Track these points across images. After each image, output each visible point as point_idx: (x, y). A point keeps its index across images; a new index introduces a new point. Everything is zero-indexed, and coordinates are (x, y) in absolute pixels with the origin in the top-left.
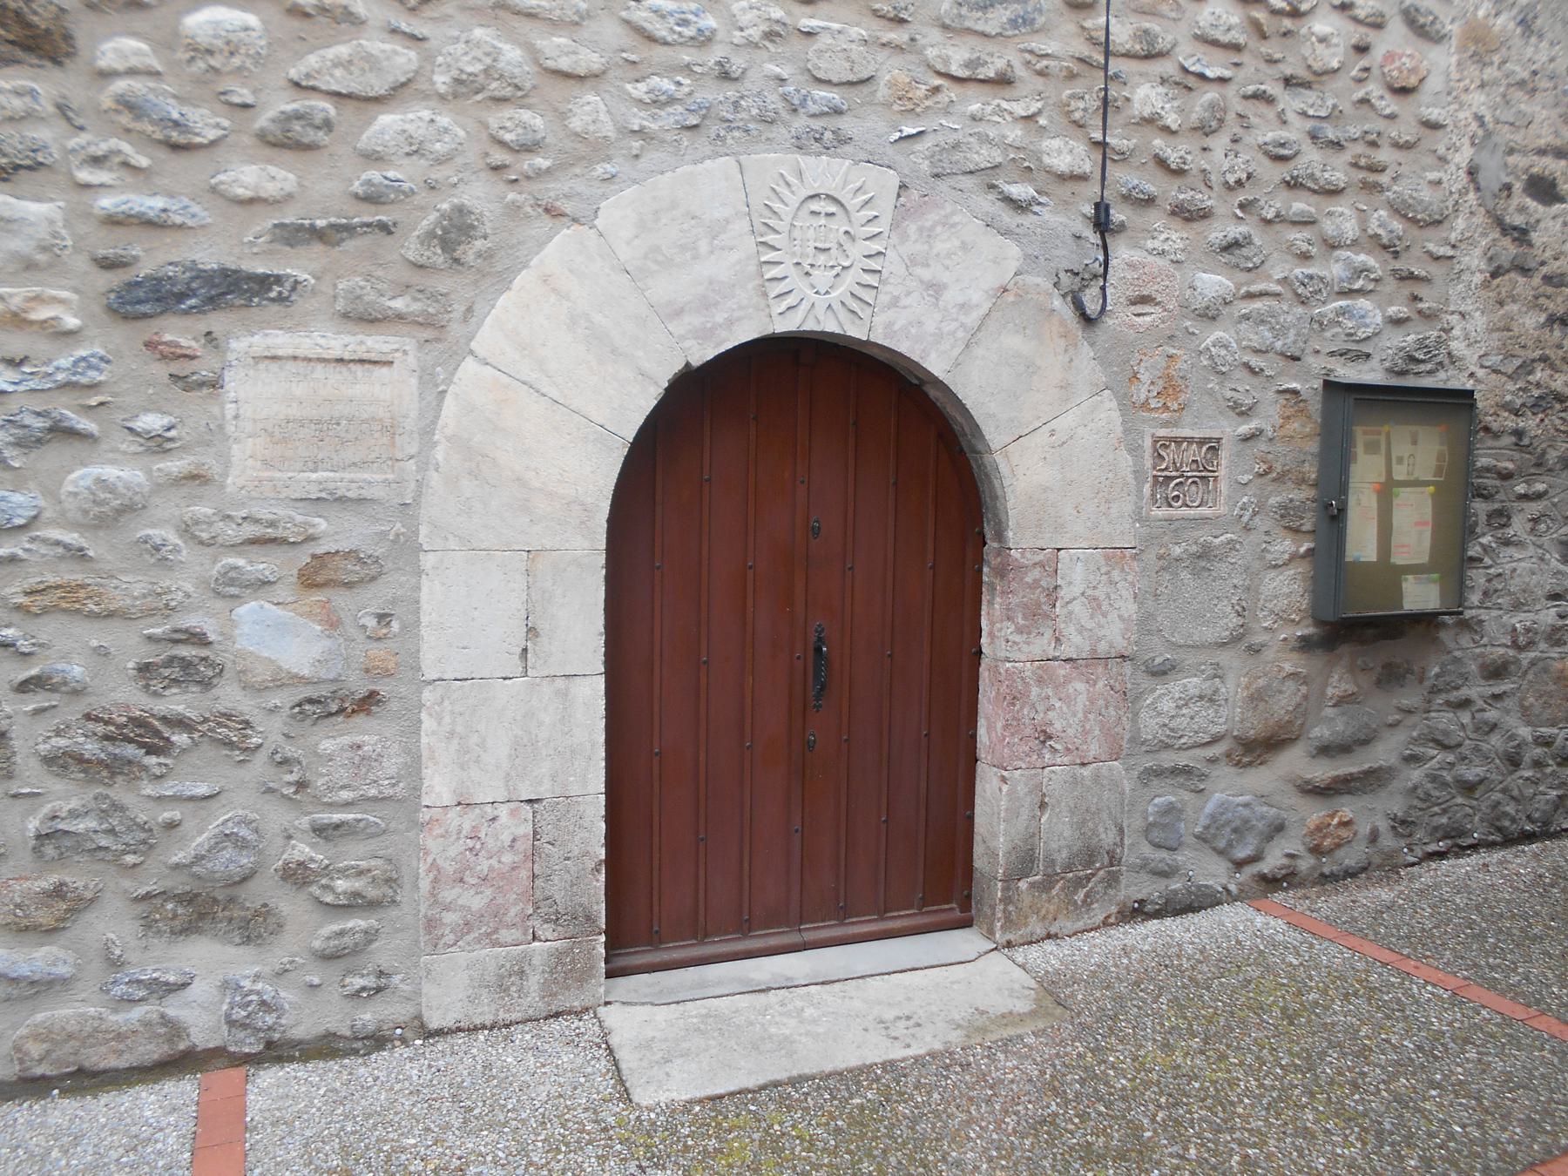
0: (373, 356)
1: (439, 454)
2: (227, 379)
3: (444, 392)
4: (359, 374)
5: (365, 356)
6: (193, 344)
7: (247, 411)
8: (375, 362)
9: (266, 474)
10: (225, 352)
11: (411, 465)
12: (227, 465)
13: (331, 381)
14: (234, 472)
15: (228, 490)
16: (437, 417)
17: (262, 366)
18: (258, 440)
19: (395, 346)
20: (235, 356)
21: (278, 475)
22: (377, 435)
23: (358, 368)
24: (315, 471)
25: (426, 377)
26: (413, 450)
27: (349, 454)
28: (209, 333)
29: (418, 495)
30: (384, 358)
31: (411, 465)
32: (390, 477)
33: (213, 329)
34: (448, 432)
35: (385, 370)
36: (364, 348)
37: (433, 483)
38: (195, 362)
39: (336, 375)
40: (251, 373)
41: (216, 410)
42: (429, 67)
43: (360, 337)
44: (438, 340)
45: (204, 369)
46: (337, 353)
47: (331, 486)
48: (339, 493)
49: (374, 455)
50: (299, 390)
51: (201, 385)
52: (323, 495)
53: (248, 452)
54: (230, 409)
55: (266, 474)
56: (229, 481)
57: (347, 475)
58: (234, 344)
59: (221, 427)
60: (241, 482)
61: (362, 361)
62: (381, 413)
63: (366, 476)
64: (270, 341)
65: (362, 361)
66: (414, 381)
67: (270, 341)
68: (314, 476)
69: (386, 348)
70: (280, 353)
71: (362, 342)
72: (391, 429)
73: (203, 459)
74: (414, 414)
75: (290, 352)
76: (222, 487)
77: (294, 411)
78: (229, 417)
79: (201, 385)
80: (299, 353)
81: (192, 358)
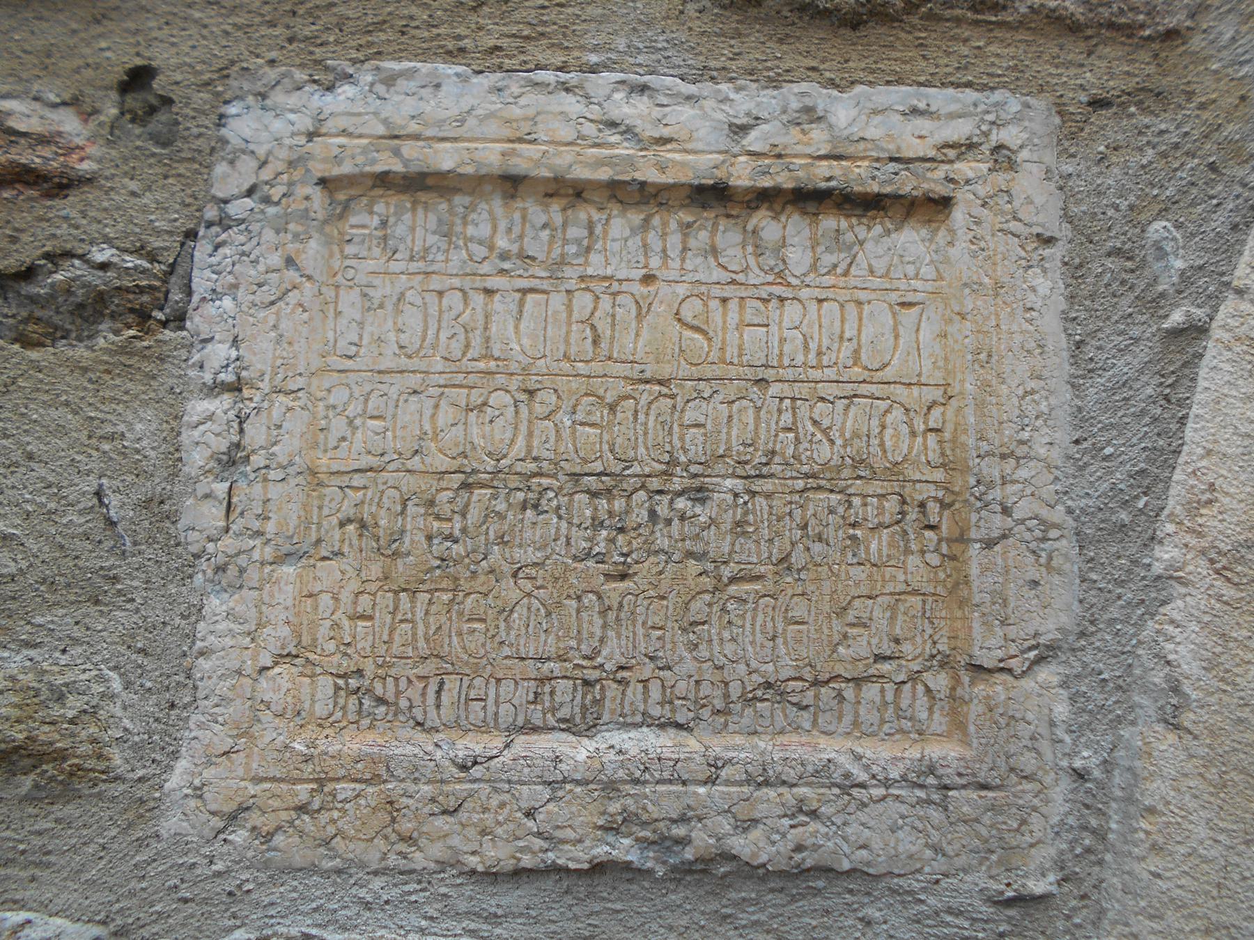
0: (859, 176)
1: (1183, 637)
2: (201, 282)
3: (1196, 331)
4: (798, 258)
5: (823, 174)
6: (69, 124)
7: (280, 432)
8: (868, 205)
9: (354, 743)
10: (204, 160)
11: (1044, 695)
12: (175, 698)
13: (667, 297)
14: (204, 732)
15: (171, 824)
16: (1166, 455)
17: (363, 221)
18: (329, 573)
19: (960, 130)
20: (245, 174)
21: (407, 746)
22: (877, 545)
23: (792, 235)
24: (584, 724)
25: (1102, 264)
26: (1053, 617)
27: (752, 643)
28: (138, 78)
29: (1089, 847)
30: (907, 184)
31: (1044, 695)
32: (946, 752)
33: (160, 56)
34: (1224, 525)
35: (911, 238)
36: (819, 138)
37: (1155, 790)
38: (69, 206)
39: (694, 259)
40: (312, 252)
41: (142, 427)
42: (1068, 21)
43: (794, 94)
44: (1150, 97)
45: (99, 239)
46: (698, 161)
47: (662, 802)
48: (701, 840)
49: (862, 645)
50: (526, 331)
51: (92, 308)
52: (624, 849)
53: (277, 635)
54: (208, 416)
55: (354, 743)
56: (176, 780)
57: (738, 747)
58: (244, 124)
59: (161, 510)
60: (228, 783)
61: (808, 199)
62: (898, 441)
63: (832, 750)
64: (401, 107)
65: (808, 199)
66: (1046, 286)
67: (401, 107)
68: (579, 752)
69: (915, 138)
70: (446, 158)
71: (811, 115)
72: (945, 515)
73: (62, 667)
74: (1049, 443)
75: (491, 156)
76: (146, 807)
77: (499, 434)
78: (197, 459)
79: (92, 308)
80: (526, 159)
81: (59, 185)
